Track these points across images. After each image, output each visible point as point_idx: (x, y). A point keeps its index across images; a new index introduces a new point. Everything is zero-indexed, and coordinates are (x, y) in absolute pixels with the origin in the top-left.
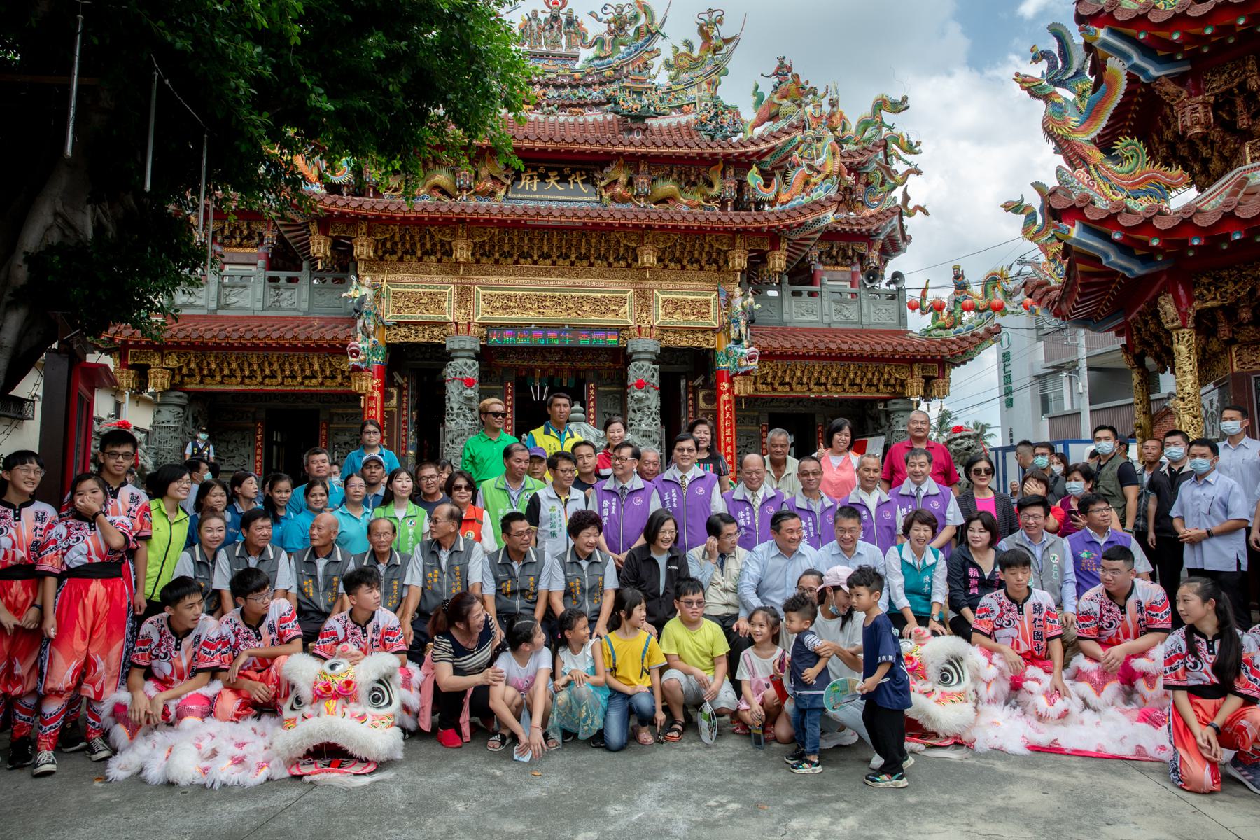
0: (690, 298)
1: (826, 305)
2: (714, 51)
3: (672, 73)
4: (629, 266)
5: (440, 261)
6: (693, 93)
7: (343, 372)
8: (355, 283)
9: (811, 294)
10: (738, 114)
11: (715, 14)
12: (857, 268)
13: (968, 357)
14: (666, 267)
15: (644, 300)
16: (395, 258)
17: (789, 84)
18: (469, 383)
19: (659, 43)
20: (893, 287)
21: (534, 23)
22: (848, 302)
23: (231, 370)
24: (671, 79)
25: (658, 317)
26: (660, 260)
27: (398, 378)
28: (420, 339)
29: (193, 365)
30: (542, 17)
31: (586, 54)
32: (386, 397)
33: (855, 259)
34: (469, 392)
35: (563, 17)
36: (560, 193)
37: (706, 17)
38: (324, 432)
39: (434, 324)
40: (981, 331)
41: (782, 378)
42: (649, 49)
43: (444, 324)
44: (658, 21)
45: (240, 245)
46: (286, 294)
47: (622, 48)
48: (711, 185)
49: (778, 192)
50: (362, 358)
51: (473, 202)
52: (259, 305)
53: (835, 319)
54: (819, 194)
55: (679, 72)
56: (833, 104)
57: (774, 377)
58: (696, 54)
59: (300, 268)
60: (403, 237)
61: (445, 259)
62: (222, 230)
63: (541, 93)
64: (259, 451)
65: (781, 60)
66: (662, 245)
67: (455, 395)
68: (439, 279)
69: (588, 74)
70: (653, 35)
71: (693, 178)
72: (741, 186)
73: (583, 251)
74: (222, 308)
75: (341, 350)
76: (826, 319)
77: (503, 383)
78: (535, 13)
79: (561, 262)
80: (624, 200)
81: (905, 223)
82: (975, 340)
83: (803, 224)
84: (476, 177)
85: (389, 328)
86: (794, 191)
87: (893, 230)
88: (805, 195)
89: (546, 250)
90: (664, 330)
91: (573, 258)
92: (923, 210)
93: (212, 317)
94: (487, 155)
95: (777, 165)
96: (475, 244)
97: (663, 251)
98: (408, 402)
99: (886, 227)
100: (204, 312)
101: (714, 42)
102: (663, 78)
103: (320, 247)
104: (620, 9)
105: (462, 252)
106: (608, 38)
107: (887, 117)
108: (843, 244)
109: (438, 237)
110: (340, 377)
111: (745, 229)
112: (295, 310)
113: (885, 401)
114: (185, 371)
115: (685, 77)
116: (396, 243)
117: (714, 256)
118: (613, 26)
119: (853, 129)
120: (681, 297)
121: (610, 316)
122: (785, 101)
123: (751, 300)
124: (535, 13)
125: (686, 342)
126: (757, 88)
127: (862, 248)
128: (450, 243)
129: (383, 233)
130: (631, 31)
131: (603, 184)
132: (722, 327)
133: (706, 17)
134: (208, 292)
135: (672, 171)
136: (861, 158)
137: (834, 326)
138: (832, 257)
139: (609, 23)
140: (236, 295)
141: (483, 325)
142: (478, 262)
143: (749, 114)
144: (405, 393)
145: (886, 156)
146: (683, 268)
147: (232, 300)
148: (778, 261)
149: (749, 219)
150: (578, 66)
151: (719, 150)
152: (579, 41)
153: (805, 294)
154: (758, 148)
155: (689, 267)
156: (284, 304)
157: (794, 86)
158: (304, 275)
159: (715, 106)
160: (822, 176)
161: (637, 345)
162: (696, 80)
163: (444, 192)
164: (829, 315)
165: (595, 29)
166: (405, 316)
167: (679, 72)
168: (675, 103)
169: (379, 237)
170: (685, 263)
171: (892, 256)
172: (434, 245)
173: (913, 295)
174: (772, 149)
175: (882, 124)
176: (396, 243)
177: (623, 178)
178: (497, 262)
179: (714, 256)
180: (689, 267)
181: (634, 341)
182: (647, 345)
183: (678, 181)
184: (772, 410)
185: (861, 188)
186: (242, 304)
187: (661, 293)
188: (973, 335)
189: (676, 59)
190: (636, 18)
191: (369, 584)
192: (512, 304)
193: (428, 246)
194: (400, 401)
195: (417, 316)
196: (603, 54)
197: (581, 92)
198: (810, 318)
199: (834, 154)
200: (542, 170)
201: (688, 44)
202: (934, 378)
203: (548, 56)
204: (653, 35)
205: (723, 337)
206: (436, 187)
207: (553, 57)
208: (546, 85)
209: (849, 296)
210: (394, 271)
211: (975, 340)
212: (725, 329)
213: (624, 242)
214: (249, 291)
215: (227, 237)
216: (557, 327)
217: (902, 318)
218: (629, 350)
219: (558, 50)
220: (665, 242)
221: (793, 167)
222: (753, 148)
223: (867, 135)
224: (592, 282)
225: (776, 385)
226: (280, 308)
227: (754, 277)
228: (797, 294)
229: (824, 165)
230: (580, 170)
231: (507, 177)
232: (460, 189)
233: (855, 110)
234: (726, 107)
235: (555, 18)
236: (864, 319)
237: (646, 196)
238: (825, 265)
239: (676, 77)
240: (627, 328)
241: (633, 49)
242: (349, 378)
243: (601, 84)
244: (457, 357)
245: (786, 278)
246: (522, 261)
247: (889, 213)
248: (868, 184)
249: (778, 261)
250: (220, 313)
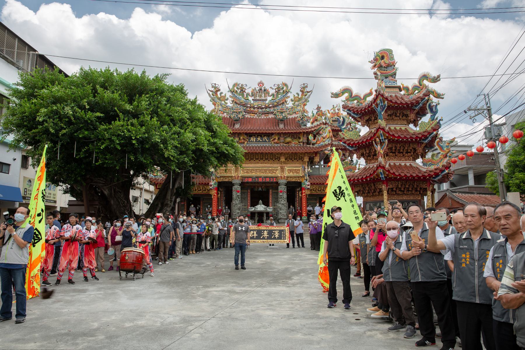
3: (293, 102)
6: (299, 108)
18: (238, 192)
19: (289, 94)
25: (286, 174)
27: (220, 189)
28: (226, 180)
30: (257, 89)
31: (269, 98)
32: (218, 194)
34: (238, 194)
35: (263, 89)
41: (399, 150)
44: (289, 88)
58: (300, 97)
67: (235, 194)
70: (287, 92)
72: (308, 139)
75: (208, 184)
77: (247, 190)
78: (255, 88)
80: (277, 143)
90: (288, 177)
98: (223, 195)
104: (278, 85)
115: (297, 103)
121: (274, 174)
124: (255, 88)
125: (294, 180)
161: (281, 181)
165: (272, 92)
177: (277, 138)
182: (283, 181)
183: (291, 138)
190: (283, 88)
191: (132, 189)
197: (268, 110)
201: (298, 94)
208: (258, 108)
212: (303, 177)
224: (269, 165)
235: (261, 89)
239: (294, 103)
243: (273, 107)
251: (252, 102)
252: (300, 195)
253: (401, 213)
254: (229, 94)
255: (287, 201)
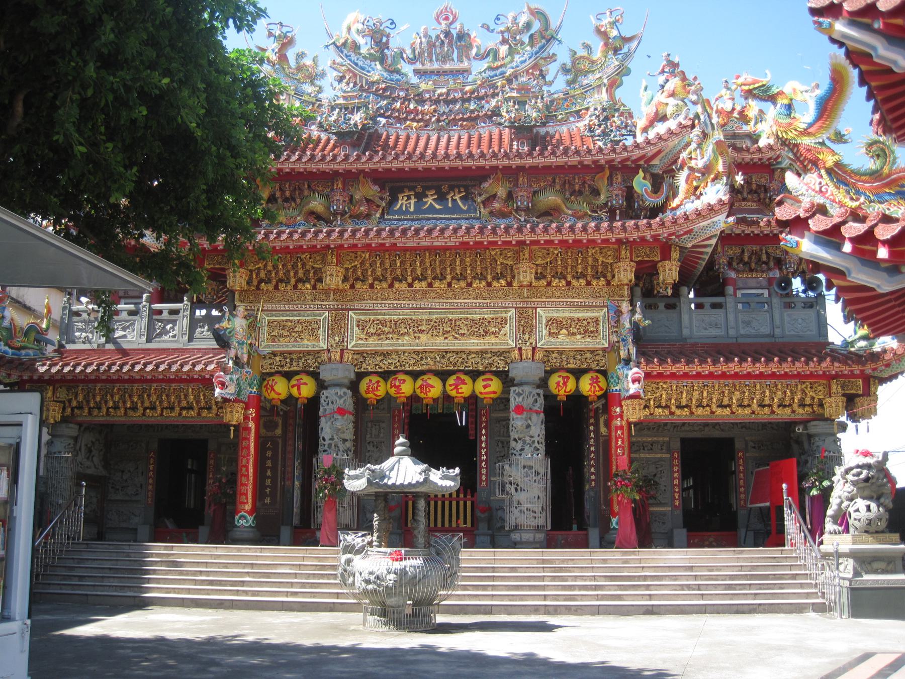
1: (731, 317)
3: (569, 77)
9: (715, 306)
19: (554, 48)
23: (114, 402)
24: (569, 83)
25: (355, 340)
33: (772, 264)
38: (212, 462)
42: (544, 55)
43: (318, 352)
48: (596, 192)
53: (742, 332)
64: (151, 481)
70: (550, 39)
96: (347, 269)
110: (214, 407)
113: (805, 422)
114: (74, 404)
121: (492, 339)
131: (479, 199)
135: (554, 181)
137: (741, 340)
172: (307, 272)
176: (270, 271)
177: (502, 192)
183: (562, 191)
184: (683, 435)
193: (301, 274)
194: (284, 431)
198: (713, 332)
200: (419, 190)
202: (858, 396)
204: (548, 41)
206: (312, 213)
210: (271, 299)
212: (614, 348)
220: (544, 258)
225: (673, 408)
230: (459, 187)
231: (381, 198)
232: (335, 214)
237: (527, 210)
251: (414, 80)
252: (603, 430)
253: (281, 223)
254: (327, 59)
255: (548, 453)
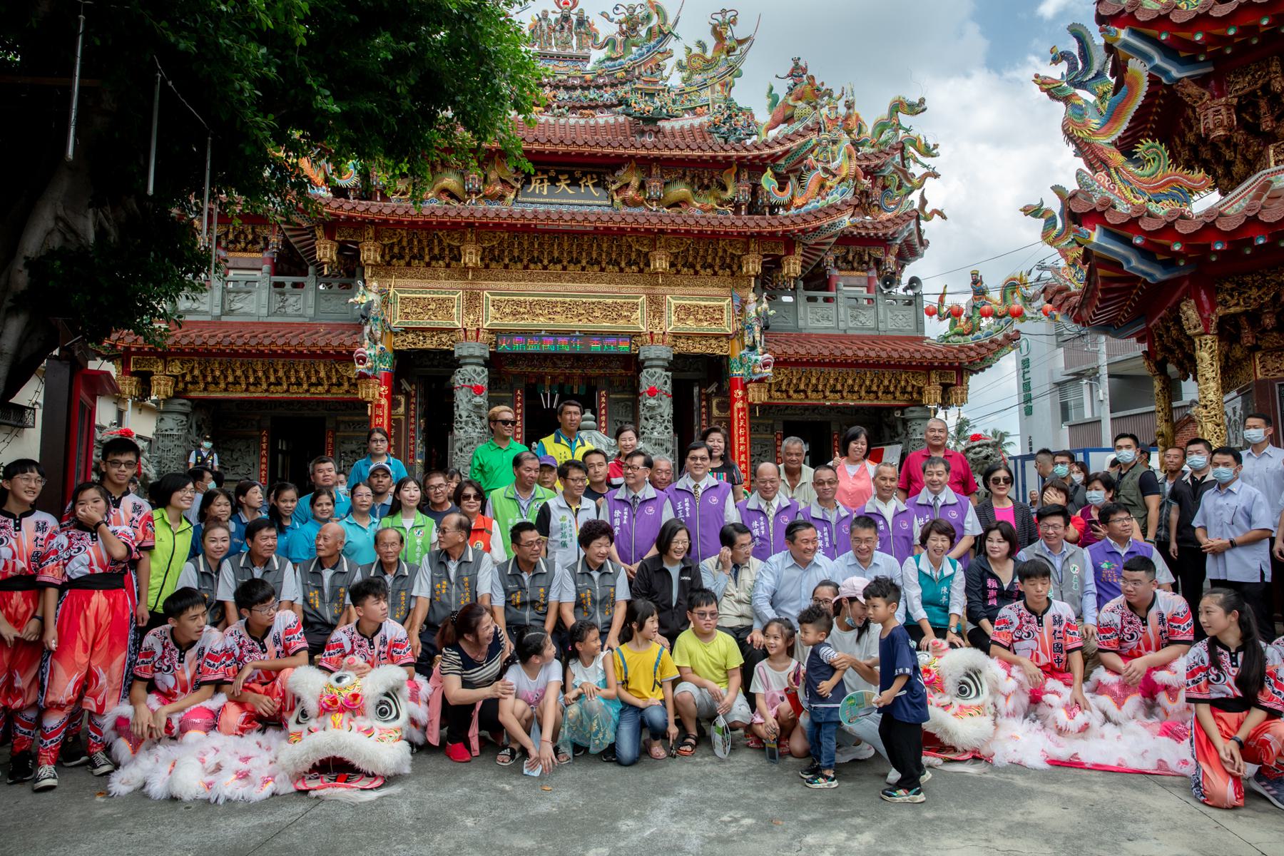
0: (703, 303)
1: (842, 310)
2: (728, 52)
3: (685, 74)
4: (641, 271)
5: (448, 266)
6: (706, 95)
7: (349, 379)
8: (362, 288)
9: (827, 300)
10: (752, 116)
11: (729, 15)
12: (873, 273)
13: (986, 364)
14: (678, 272)
15: (656, 305)
16: (402, 262)
17: (804, 86)
18: (478, 390)
19: (671, 44)
20: (910, 292)
21: (544, 24)
22: (864, 308)
23: (235, 377)
24: (684, 81)
25: (671, 323)
26: (672, 265)
27: (406, 386)
28: (428, 345)
29: (196, 372)
30: (552, 17)
31: (597, 55)
32: (393, 404)
33: (872, 264)
34: (478, 400)
35: (574, 18)
36: (570, 197)
37: (720, 18)
38: (330, 440)
39: (442, 330)
40: (1000, 337)
41: (797, 385)
42: (661, 50)
43: (453, 330)
44: (671, 21)
45: (245, 250)
46: (292, 300)
47: (634, 49)
48: (724, 188)
49: (793, 196)
50: (369, 364)
51: (482, 206)
52: (264, 311)
53: (851, 325)
54: (834, 198)
55: (692, 74)
56: (849, 106)
57: (789, 385)
58: (709, 55)
59: (305, 274)
60: (410, 242)
61: (454, 264)
62: (226, 234)
63: (551, 95)
64: (264, 460)
65: (796, 61)
66: (674, 250)
67: (464, 402)
68: (447, 284)
69: (600, 76)
70: (665, 35)
71: (706, 181)
72: (755, 189)
73: (594, 256)
74: (227, 314)
75: (347, 357)
76: (842, 325)
77: (513, 390)
78: (545, 14)
79: (571, 267)
80: (636, 204)
81: (922, 227)
82: (994, 346)
83: (818, 228)
84: (485, 180)
85: (396, 334)
86: (809, 194)
87: (910, 235)
88: (821, 199)
89: (556, 254)
90: (676, 336)
91: (584, 263)
92: (941, 214)
93: (216, 323)
94: (496, 158)
95: (791, 168)
96: (484, 249)
97: (676, 256)
98: (416, 409)
99: (903, 231)
100: (208, 318)
101: (727, 42)
102: (675, 80)
103: (326, 251)
104: (632, 9)
105: (471, 257)
106: (620, 38)
107: (904, 119)
108: (859, 249)
109: (446, 241)
110: (346, 384)
111: (759, 233)
112: (300, 316)
113: (902, 408)
114: (188, 378)
115: (698, 78)
116: (403, 248)
117: (728, 261)
118: (624, 26)
119: (870, 132)
120: (694, 303)
121: (622, 322)
122: (800, 103)
123: (765, 305)
124: (545, 14)
125: (699, 348)
126: (771, 89)
127: (878, 253)
128: (458, 248)
129: (390, 237)
130: (643, 31)
131: (614, 187)
132: (736, 333)
133: (720, 18)
134: (212, 298)
135: (684, 174)
136: (877, 162)
137: (850, 332)
138: (848, 262)
139: (620, 23)
140: (240, 301)
141: (492, 331)
142: (487, 266)
143: (763, 117)
144: (413, 400)
145: (903, 159)
146: (696, 273)
147: (236, 306)
148: (793, 266)
149: (763, 224)
150: (589, 67)
151: (733, 153)
152: (590, 42)
153: (820, 300)
154: (772, 151)
155: (702, 272)
156: (289, 310)
157: (809, 88)
158: (310, 280)
159: (729, 108)
160: (838, 179)
161: (649, 352)
162: (709, 82)
163: (452, 195)
164: (845, 321)
165: (606, 30)
166: (413, 322)
167: (692, 74)
168: (687, 105)
169: (386, 241)
170: (698, 268)
171: (909, 261)
172: (442, 250)
173: (930, 300)
174: (787, 152)
175: (899, 126)
176: (403, 248)
177: (635, 182)
178: (506, 267)
179: (728, 261)
180: (702, 272)
181: (646, 348)
182: (659, 352)
183: (691, 184)
184: (786, 418)
185: (877, 191)
186: (246, 309)
187: (673, 299)
188: (992, 342)
189: (689, 60)
190: (648, 18)
192: (522, 310)
193: (436, 251)
194: (407, 409)
195: (425, 322)
196: (614, 55)
197: (592, 94)
198: (826, 324)
199: (850, 157)
200: (552, 174)
201: (701, 45)
202: (951, 385)
203: (558, 57)
204: (666, 35)
205: (736, 344)
206: (444, 190)
207: (564, 58)
208: (556, 87)
209: (865, 302)
210: (402, 276)
211: (994, 346)
212: (739, 335)
213: (636, 247)
214: (254, 296)
215: (231, 242)
216: (567, 333)
217: (919, 324)
218: (641, 357)
219: (569, 51)
220: (678, 247)
221: (809, 170)
222: (767, 151)
223: (883, 138)
224: (603, 287)
225: (791, 392)
226: (285, 314)
227: (769, 282)
228: (812, 299)
229: (839, 168)
230: (591, 173)
231: (517, 180)
232: (469, 193)
233: (871, 112)
234: (740, 109)
235: (566, 18)
236: (881, 325)
237: (659, 200)
238: (841, 270)
239: (689, 78)
240: (639, 334)
241: (645, 50)
242: (356, 385)
243: (613, 85)
244: (466, 364)
245: (801, 284)
246: (532, 266)
247: (906, 217)
248: (884, 188)
249: (793, 266)
250: (224, 319)
